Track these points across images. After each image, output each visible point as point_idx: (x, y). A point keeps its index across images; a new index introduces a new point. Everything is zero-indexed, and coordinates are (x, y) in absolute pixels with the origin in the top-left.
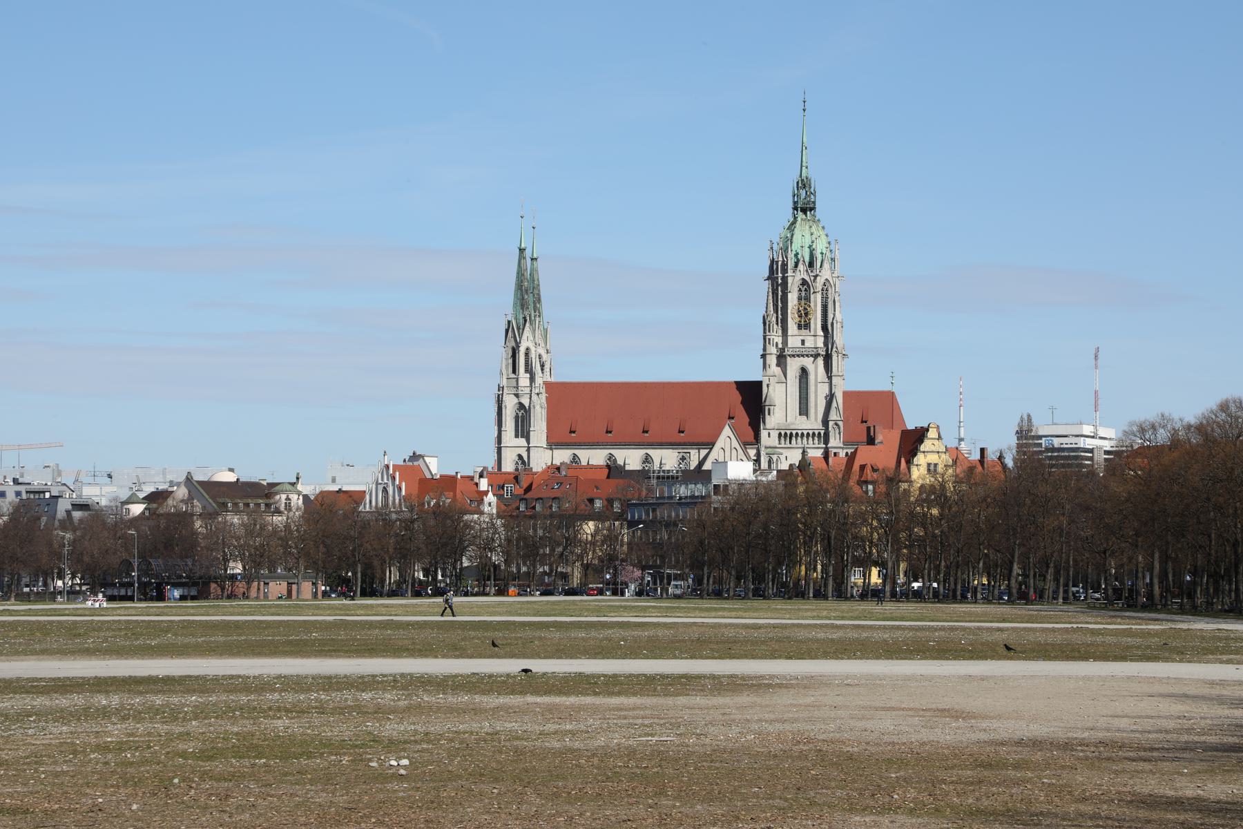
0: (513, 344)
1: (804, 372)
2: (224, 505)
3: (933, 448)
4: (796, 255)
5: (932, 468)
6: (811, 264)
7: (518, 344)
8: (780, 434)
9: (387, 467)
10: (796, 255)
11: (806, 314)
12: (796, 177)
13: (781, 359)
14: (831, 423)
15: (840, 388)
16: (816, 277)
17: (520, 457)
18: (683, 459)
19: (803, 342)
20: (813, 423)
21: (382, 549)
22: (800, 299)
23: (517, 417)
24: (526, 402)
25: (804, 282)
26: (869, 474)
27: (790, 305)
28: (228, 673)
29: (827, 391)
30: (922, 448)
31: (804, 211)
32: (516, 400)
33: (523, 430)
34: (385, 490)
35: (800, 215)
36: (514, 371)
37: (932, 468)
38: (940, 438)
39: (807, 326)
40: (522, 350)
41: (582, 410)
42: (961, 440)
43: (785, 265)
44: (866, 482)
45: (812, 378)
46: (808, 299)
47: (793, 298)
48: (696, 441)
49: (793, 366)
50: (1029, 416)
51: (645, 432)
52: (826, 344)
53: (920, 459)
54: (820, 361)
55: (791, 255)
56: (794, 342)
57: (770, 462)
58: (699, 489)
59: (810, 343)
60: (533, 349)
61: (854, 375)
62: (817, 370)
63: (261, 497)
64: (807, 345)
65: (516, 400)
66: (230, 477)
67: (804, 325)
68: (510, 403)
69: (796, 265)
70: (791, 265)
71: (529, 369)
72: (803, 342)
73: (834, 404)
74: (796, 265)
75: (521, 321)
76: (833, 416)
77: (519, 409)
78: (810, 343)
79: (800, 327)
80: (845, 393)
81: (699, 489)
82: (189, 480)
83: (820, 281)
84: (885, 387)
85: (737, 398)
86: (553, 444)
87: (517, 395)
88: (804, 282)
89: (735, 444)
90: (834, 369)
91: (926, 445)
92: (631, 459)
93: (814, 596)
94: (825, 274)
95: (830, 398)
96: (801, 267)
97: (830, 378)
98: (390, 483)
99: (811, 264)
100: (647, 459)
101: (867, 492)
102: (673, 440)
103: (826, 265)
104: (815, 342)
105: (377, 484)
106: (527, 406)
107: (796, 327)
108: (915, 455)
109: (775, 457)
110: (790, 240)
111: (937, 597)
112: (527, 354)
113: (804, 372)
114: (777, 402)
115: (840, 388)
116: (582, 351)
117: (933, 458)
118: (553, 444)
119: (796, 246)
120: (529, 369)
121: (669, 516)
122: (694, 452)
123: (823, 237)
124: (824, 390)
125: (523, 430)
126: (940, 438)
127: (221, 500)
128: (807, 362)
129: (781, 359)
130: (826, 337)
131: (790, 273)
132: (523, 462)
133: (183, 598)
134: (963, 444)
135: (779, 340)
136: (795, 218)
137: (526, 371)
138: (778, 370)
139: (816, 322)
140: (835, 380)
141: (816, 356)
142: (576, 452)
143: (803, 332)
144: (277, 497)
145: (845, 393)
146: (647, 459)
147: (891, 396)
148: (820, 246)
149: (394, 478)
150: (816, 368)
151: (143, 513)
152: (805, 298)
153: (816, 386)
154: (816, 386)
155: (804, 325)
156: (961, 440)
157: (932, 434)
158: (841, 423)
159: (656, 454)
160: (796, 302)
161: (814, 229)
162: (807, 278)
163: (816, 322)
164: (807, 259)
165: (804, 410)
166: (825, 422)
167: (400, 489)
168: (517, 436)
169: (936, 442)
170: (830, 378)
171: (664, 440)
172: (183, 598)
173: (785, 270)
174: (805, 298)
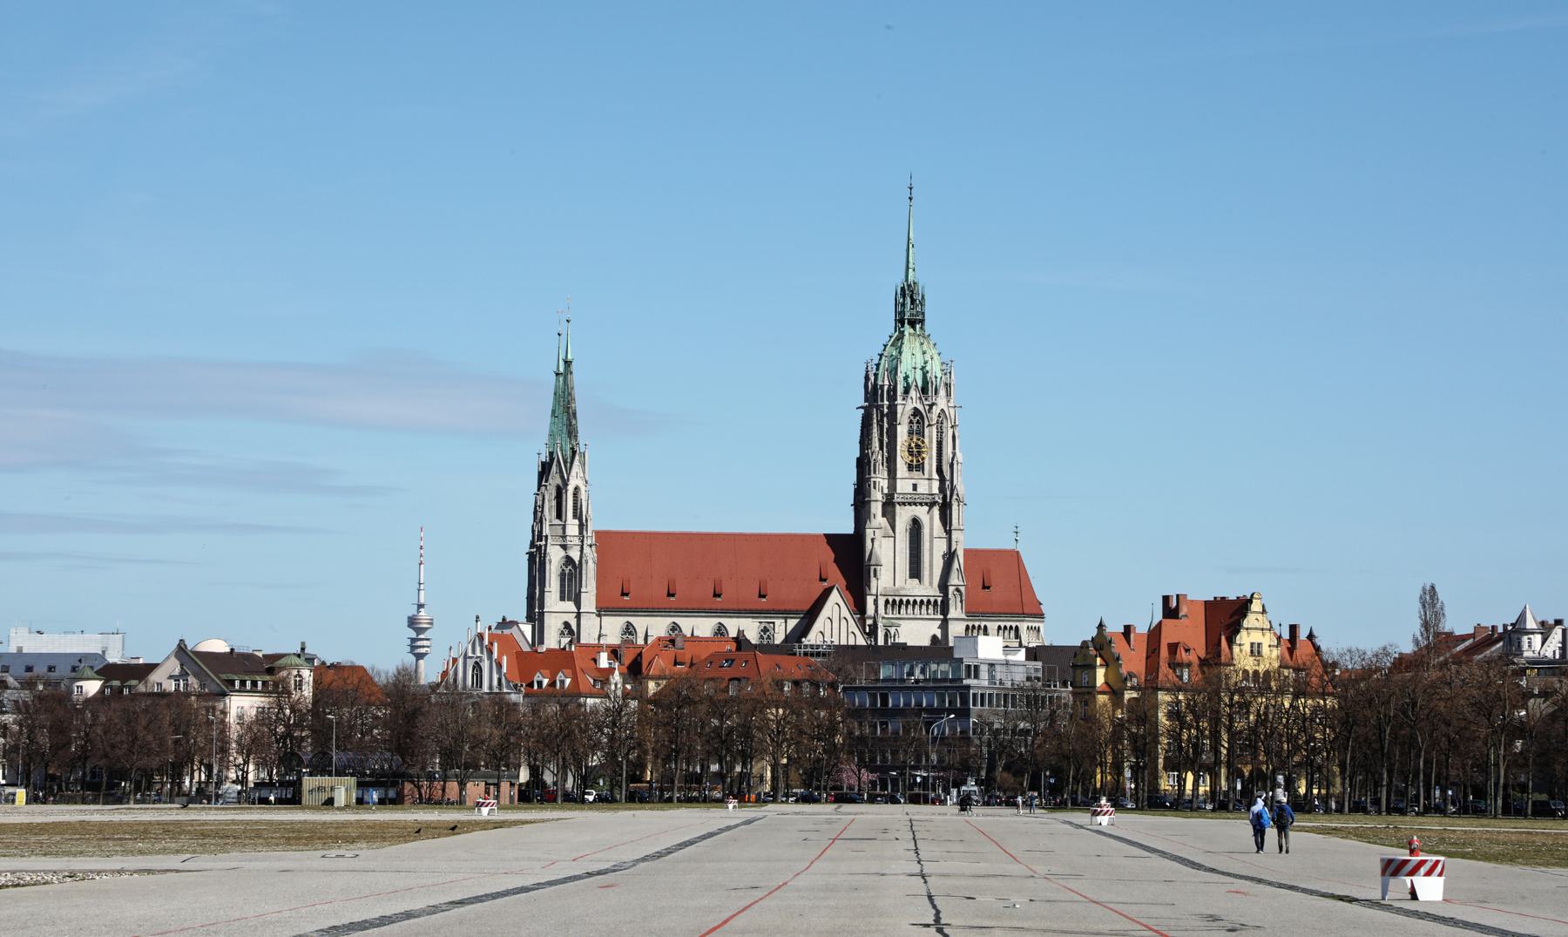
0: (559, 481)
1: (916, 524)
2: (232, 682)
3: (1257, 625)
4: (906, 378)
6: (924, 390)
7: (565, 483)
8: (887, 602)
9: (481, 636)
10: (906, 378)
11: (919, 453)
12: (899, 281)
13: (889, 506)
14: (951, 589)
15: (961, 542)
16: (931, 406)
17: (567, 625)
18: (765, 630)
19: (915, 487)
20: (927, 588)
21: (384, 743)
22: (910, 433)
23: (562, 575)
25: (916, 412)
28: (1505, 868)
29: (944, 548)
30: (1246, 624)
31: (912, 324)
32: (562, 553)
33: (570, 590)
34: (477, 667)
35: (908, 329)
36: (559, 516)
38: (1264, 611)
39: (920, 467)
40: (571, 489)
41: (643, 569)
42: (420, 606)
44: (1181, 665)
45: (926, 531)
46: (921, 433)
47: (902, 431)
49: (903, 516)
50: (1433, 587)
51: (716, 595)
52: (942, 489)
53: (1245, 639)
54: (936, 510)
55: (900, 377)
56: (904, 486)
57: (886, 636)
58: (943, 669)
59: (923, 488)
60: (583, 489)
61: (978, 530)
62: (931, 521)
63: (259, 673)
64: (920, 490)
66: (220, 647)
67: (916, 466)
68: (555, 556)
69: (907, 391)
70: (900, 389)
71: (577, 514)
72: (915, 487)
73: (956, 565)
74: (907, 391)
75: (569, 453)
76: (955, 580)
77: (566, 564)
78: (923, 488)
79: (910, 468)
80: (966, 552)
81: (943, 669)
82: (181, 651)
83: (936, 410)
84: (1007, 544)
85: (830, 555)
86: (602, 610)
87: (564, 547)
88: (916, 412)
89: (845, 613)
90: (955, 521)
91: (1250, 621)
92: (751, 629)
94: (941, 402)
95: (950, 557)
96: (913, 393)
97: (949, 533)
98: (485, 657)
99: (924, 390)
100: (629, 629)
101: (1181, 678)
105: (466, 657)
109: (892, 630)
112: (576, 495)
113: (916, 524)
115: (961, 542)
116: (629, 492)
117: (1256, 637)
118: (602, 610)
119: (903, 369)
120: (577, 514)
122: (779, 622)
123: (936, 357)
124: (941, 547)
125: (570, 590)
126: (1264, 611)
127: (224, 676)
128: (921, 512)
129: (889, 506)
130: (942, 480)
131: (899, 401)
132: (571, 632)
133: (382, 802)
134: (423, 612)
135: (884, 484)
137: (575, 516)
138: (883, 521)
140: (955, 535)
141: (931, 505)
143: (915, 474)
144: (284, 673)
145: (966, 552)
146: (629, 629)
147: (1016, 555)
148: (935, 369)
149: (490, 652)
150: (931, 519)
151: (102, 691)
152: (917, 430)
155: (916, 466)
156: (420, 606)
157: (1256, 606)
159: (640, 623)
160: (906, 437)
161: (925, 347)
162: (920, 407)
165: (915, 572)
166: (944, 586)
167: (499, 666)
168: (562, 599)
169: (1260, 617)
170: (949, 533)
174: (917, 430)
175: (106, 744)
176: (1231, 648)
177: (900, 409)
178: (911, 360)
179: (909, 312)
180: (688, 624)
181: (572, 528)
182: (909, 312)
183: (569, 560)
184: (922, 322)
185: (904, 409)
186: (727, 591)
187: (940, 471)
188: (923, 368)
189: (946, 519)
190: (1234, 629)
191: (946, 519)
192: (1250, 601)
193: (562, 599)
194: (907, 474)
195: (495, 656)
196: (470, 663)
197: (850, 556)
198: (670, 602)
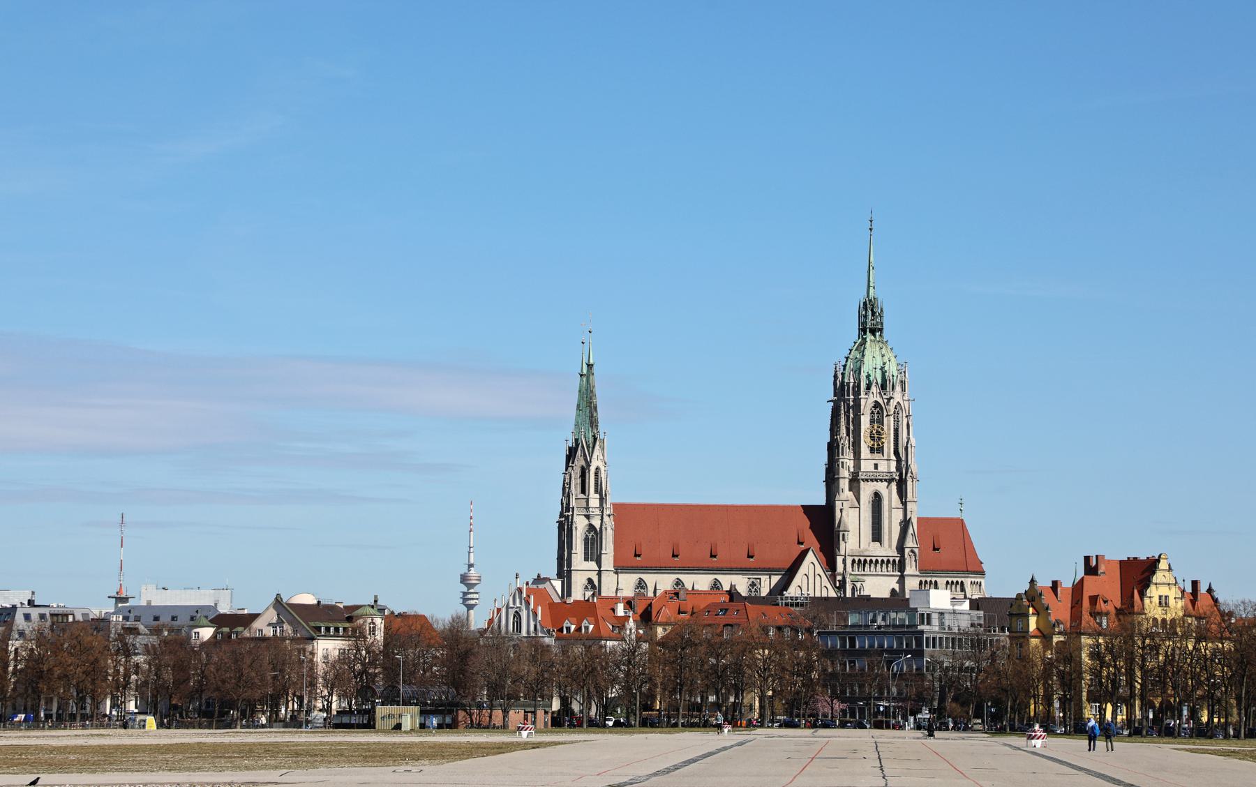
0: (583, 463)
1: (877, 497)
4: (868, 376)
5: (1163, 600)
6: (883, 387)
7: (589, 465)
8: (854, 561)
9: (520, 590)
10: (868, 376)
11: (879, 439)
12: (862, 297)
13: (855, 482)
14: (907, 551)
16: (889, 400)
17: (590, 581)
18: (753, 585)
19: (876, 466)
20: (887, 550)
21: (440, 676)
22: (872, 422)
23: (586, 539)
24: (596, 523)
25: (877, 405)
26: (1102, 606)
27: (863, 427)
30: (1154, 579)
31: (873, 332)
32: (586, 522)
33: (593, 550)
35: (869, 337)
36: (583, 491)
37: (1163, 600)
38: (1170, 569)
40: (593, 469)
41: (652, 535)
42: (471, 566)
43: (857, 387)
44: (1100, 614)
45: (885, 503)
46: (881, 422)
47: (865, 421)
48: (767, 566)
49: (867, 490)
51: (712, 556)
52: (899, 468)
53: (1154, 592)
54: (894, 486)
55: (863, 375)
56: (867, 466)
57: (853, 589)
59: (883, 467)
60: (602, 469)
61: (928, 502)
62: (890, 495)
63: (341, 621)
64: (880, 469)
65: (586, 522)
67: (877, 449)
68: (580, 524)
69: (869, 387)
71: (598, 490)
72: (876, 466)
73: (910, 531)
74: (869, 387)
75: (591, 440)
76: (910, 543)
77: (589, 531)
78: (883, 467)
79: (872, 450)
82: (278, 603)
84: (954, 514)
86: (619, 569)
87: (588, 517)
89: (819, 570)
91: (1158, 577)
92: (741, 584)
93: (1246, 736)
94: (898, 396)
95: (905, 524)
96: (874, 389)
97: (904, 504)
98: (523, 607)
99: (883, 387)
100: (641, 584)
101: (1100, 624)
102: (705, 565)
103: (898, 388)
104: (889, 466)
105: (508, 607)
106: (598, 527)
107: (868, 451)
108: (1148, 586)
109: (858, 585)
110: (860, 362)
111: (1136, 731)
112: (596, 474)
113: (877, 497)
114: (850, 528)
115: (915, 511)
116: (639, 472)
117: (1164, 591)
121: (872, 646)
122: (764, 578)
123: (893, 359)
124: (898, 516)
125: (593, 550)
126: (1170, 569)
127: (312, 624)
128: (881, 487)
129: (855, 482)
130: (899, 460)
131: (863, 395)
132: (593, 587)
133: (440, 726)
135: (851, 464)
136: (865, 340)
137: (596, 492)
138: (850, 495)
139: (889, 447)
140: (909, 506)
141: (890, 481)
142: (718, 577)
143: (876, 455)
144: (360, 621)
145: (919, 519)
146: (641, 584)
148: (892, 369)
149: (528, 603)
150: (890, 493)
153: (890, 512)
154: (890, 512)
155: (877, 449)
156: (471, 566)
157: (1163, 565)
158: (916, 550)
159: (650, 579)
161: (884, 351)
162: (880, 401)
163: (889, 447)
164: (880, 382)
165: (877, 536)
166: (901, 548)
167: (535, 614)
168: (586, 559)
169: (1166, 574)
170: (904, 504)
171: (734, 565)
172: (440, 726)
173: (857, 392)
175: (44, 673)
176: (1142, 600)
177: (863, 402)
178: (872, 362)
179: (870, 323)
180: (689, 580)
181: (594, 501)
182: (870, 323)
183: (591, 527)
184: (881, 330)
185: (867, 403)
186: (682, 552)
187: (896, 453)
188: (882, 369)
189: (902, 493)
190: (1145, 584)
191: (902, 493)
192: (1158, 561)
193: (586, 559)
194: (869, 456)
195: (532, 607)
196: (511, 612)
197: (823, 524)
198: (675, 562)
